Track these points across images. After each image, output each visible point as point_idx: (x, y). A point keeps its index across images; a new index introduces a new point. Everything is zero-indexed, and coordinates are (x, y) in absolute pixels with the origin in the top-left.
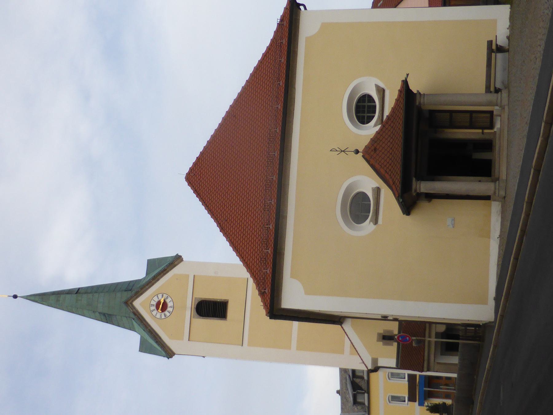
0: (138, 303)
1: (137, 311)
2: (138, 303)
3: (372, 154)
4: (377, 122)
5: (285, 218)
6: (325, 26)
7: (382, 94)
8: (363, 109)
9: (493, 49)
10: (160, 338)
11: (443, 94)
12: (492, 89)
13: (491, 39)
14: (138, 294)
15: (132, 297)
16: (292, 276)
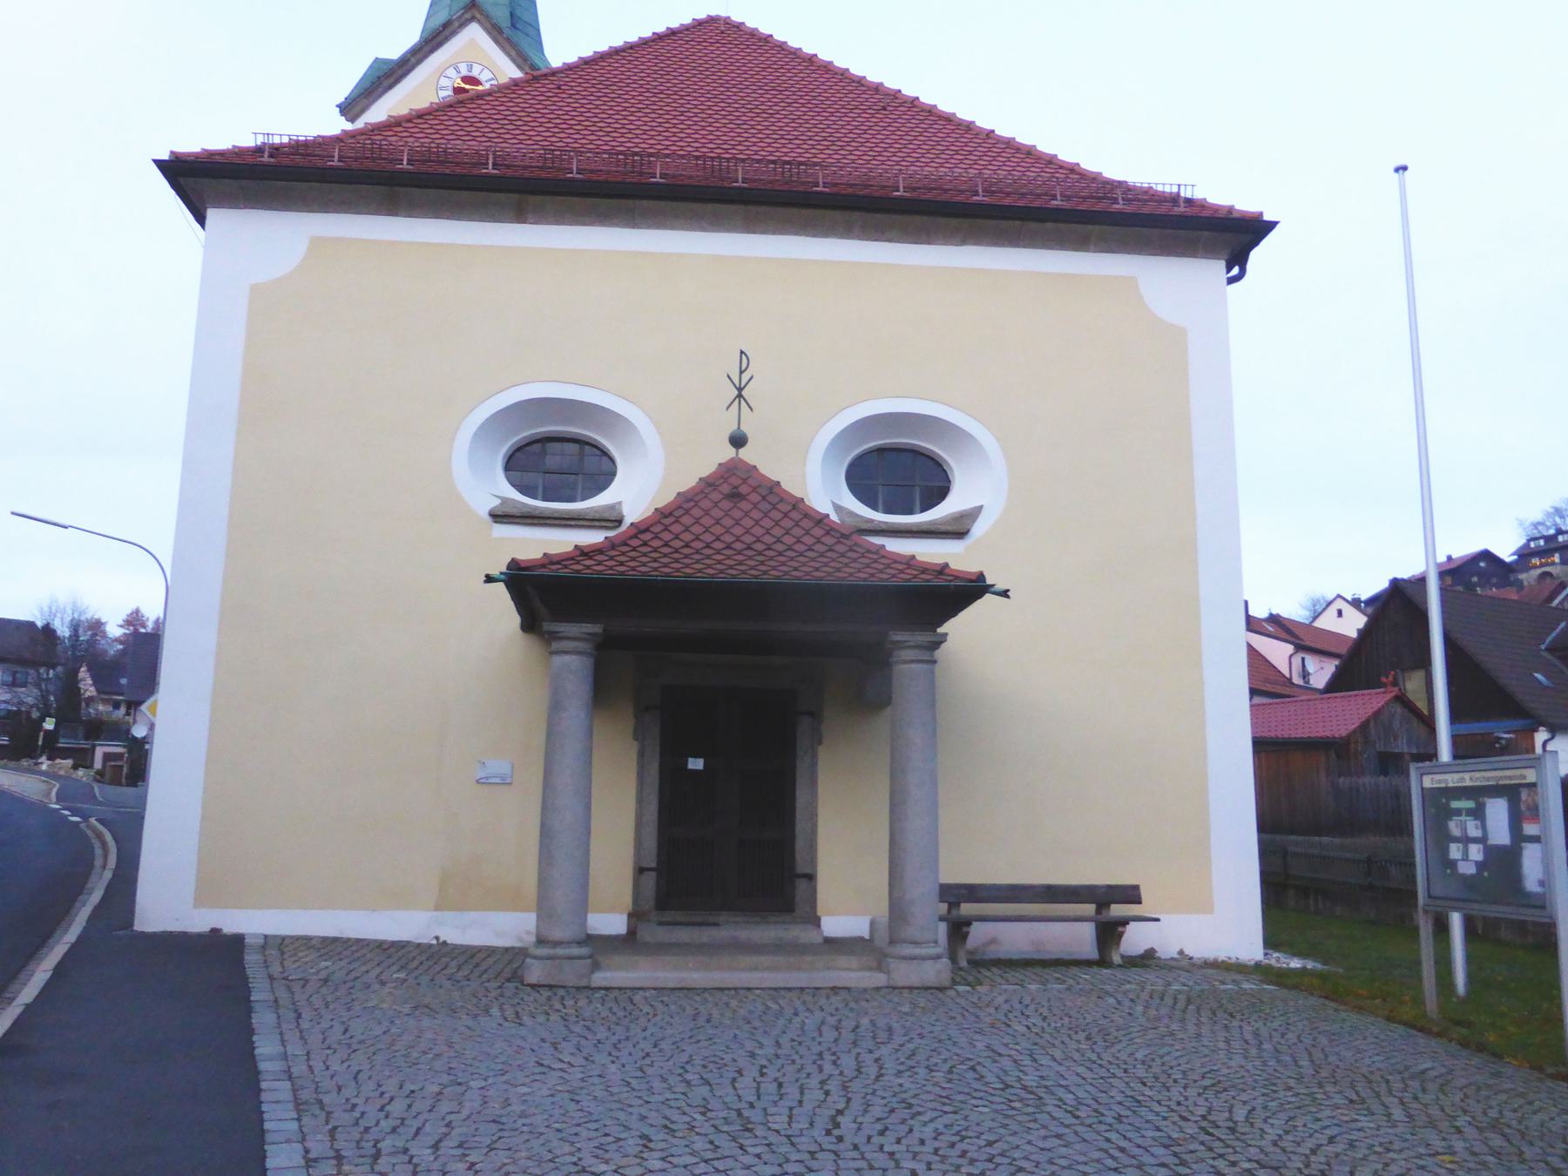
0: (474, 36)
1: (454, 33)
2: (474, 36)
3: (737, 489)
4: (851, 514)
5: (520, 216)
6: (1174, 339)
7: (949, 528)
8: (901, 469)
9: (1109, 906)
10: (390, 87)
11: (934, 732)
12: (967, 909)
13: (1145, 894)
14: (495, 32)
15: (487, 17)
16: (316, 243)
